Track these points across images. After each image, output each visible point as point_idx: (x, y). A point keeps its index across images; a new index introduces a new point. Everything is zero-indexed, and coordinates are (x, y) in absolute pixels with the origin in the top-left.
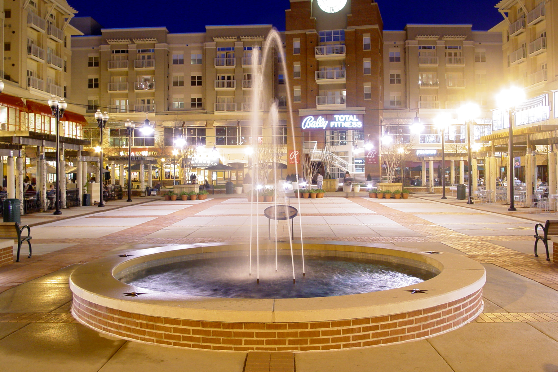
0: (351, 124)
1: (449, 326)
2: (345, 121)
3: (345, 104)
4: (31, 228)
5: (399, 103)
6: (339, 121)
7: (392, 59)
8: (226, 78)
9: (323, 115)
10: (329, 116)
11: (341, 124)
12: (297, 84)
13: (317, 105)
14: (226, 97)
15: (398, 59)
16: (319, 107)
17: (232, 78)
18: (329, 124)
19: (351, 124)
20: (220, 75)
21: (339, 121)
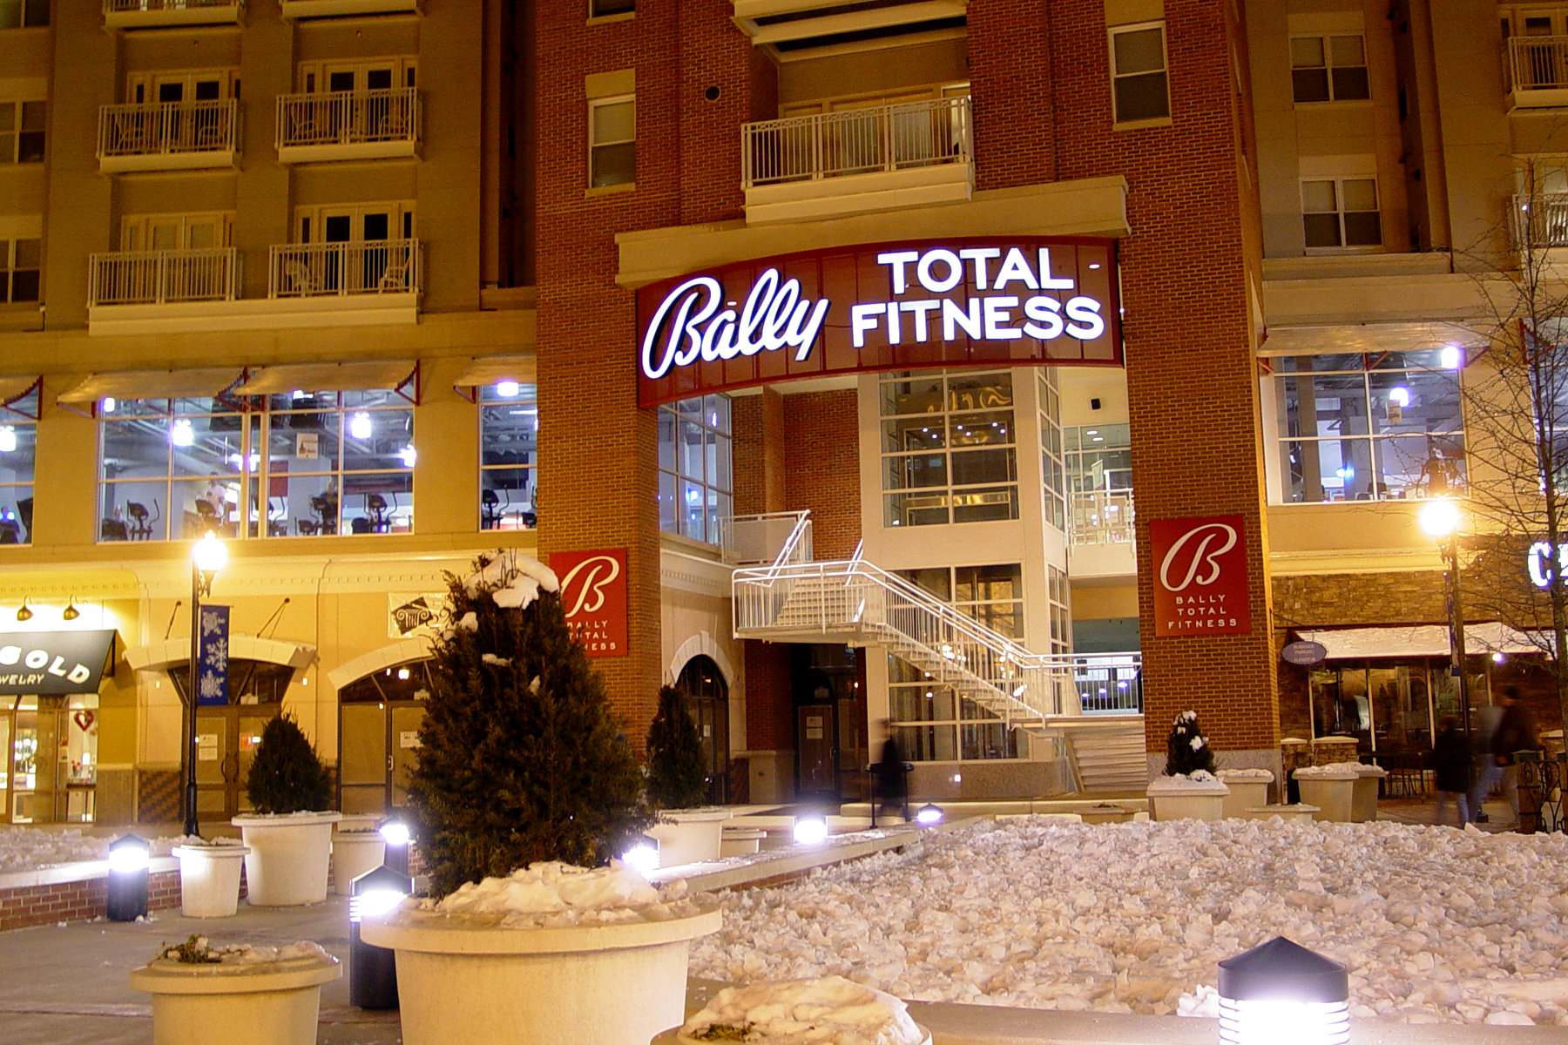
0: (1018, 317)
1: (1063, 623)
2: (964, 293)
3: (963, 168)
4: (383, 790)
5: (1366, 230)
6: (916, 290)
7: (1309, 86)
8: (357, 228)
9: (787, 265)
10: (837, 268)
11: (934, 318)
12: (609, 63)
13: (751, 192)
14: (181, 221)
15: (1353, 84)
16: (771, 205)
17: (394, 226)
18: (833, 330)
19: (1018, 317)
20: (319, 213)
21: (916, 290)
